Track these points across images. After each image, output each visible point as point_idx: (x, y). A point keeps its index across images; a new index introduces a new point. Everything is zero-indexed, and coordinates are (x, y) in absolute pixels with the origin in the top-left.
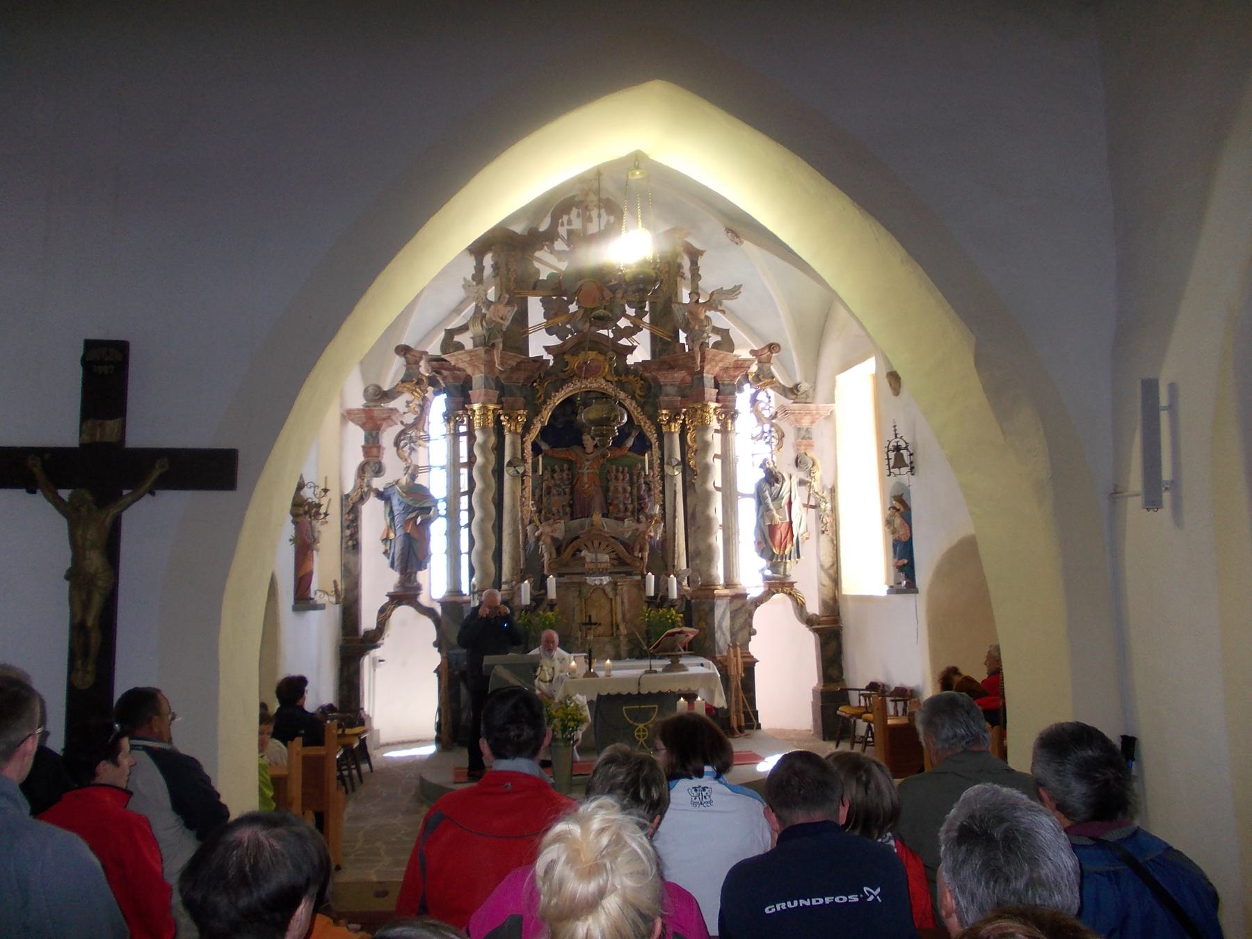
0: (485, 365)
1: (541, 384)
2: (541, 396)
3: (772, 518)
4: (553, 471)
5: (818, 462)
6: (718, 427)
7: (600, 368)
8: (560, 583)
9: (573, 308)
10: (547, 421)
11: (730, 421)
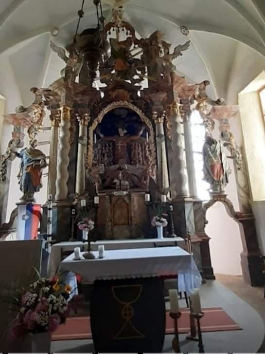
1: (98, 104)
4: (106, 146)
5: (234, 135)
6: (181, 120)
9: (113, 72)
11: (187, 116)
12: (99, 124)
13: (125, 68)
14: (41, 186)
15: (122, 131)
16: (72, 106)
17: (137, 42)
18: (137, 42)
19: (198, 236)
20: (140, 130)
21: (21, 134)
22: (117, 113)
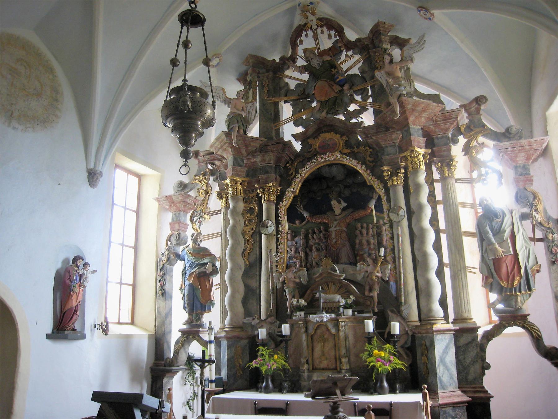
3: (495, 251)
5: (541, 196)
7: (336, 144)
9: (314, 104)
11: (446, 168)
13: (333, 95)
14: (213, 305)
15: (337, 204)
16: (244, 175)
17: (350, 45)
18: (350, 45)
19: (462, 392)
21: (182, 225)
22: (326, 172)
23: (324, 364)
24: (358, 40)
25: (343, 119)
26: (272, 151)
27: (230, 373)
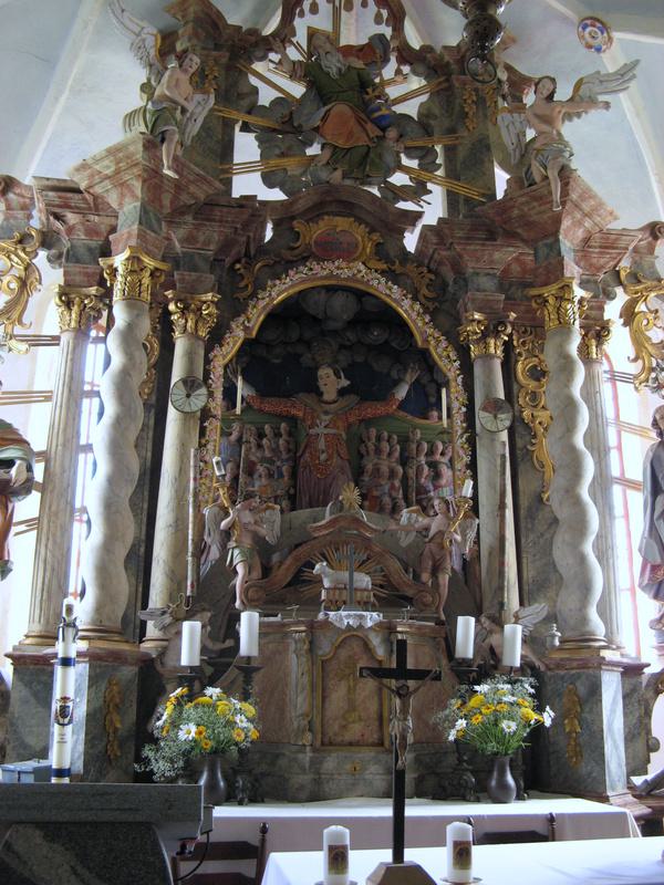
0: (144, 181)
1: (249, 266)
2: (247, 286)
4: (261, 435)
7: (357, 246)
8: (269, 625)
10: (256, 328)
11: (594, 342)
12: (247, 343)
13: (363, 141)
15: (333, 377)
17: (406, 55)
18: (406, 55)
19: (634, 796)
20: (397, 383)
23: (355, 731)
24: (426, 49)
25: (378, 194)
26: (221, 221)
27: (90, 751)
